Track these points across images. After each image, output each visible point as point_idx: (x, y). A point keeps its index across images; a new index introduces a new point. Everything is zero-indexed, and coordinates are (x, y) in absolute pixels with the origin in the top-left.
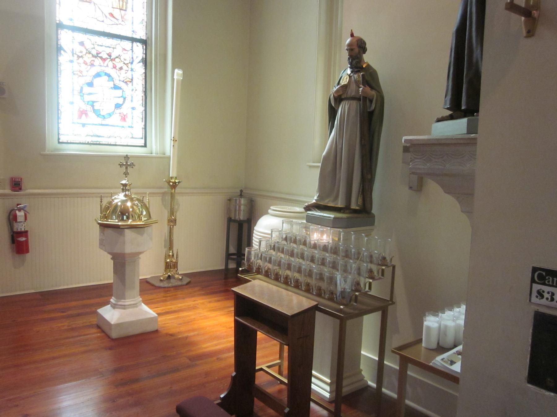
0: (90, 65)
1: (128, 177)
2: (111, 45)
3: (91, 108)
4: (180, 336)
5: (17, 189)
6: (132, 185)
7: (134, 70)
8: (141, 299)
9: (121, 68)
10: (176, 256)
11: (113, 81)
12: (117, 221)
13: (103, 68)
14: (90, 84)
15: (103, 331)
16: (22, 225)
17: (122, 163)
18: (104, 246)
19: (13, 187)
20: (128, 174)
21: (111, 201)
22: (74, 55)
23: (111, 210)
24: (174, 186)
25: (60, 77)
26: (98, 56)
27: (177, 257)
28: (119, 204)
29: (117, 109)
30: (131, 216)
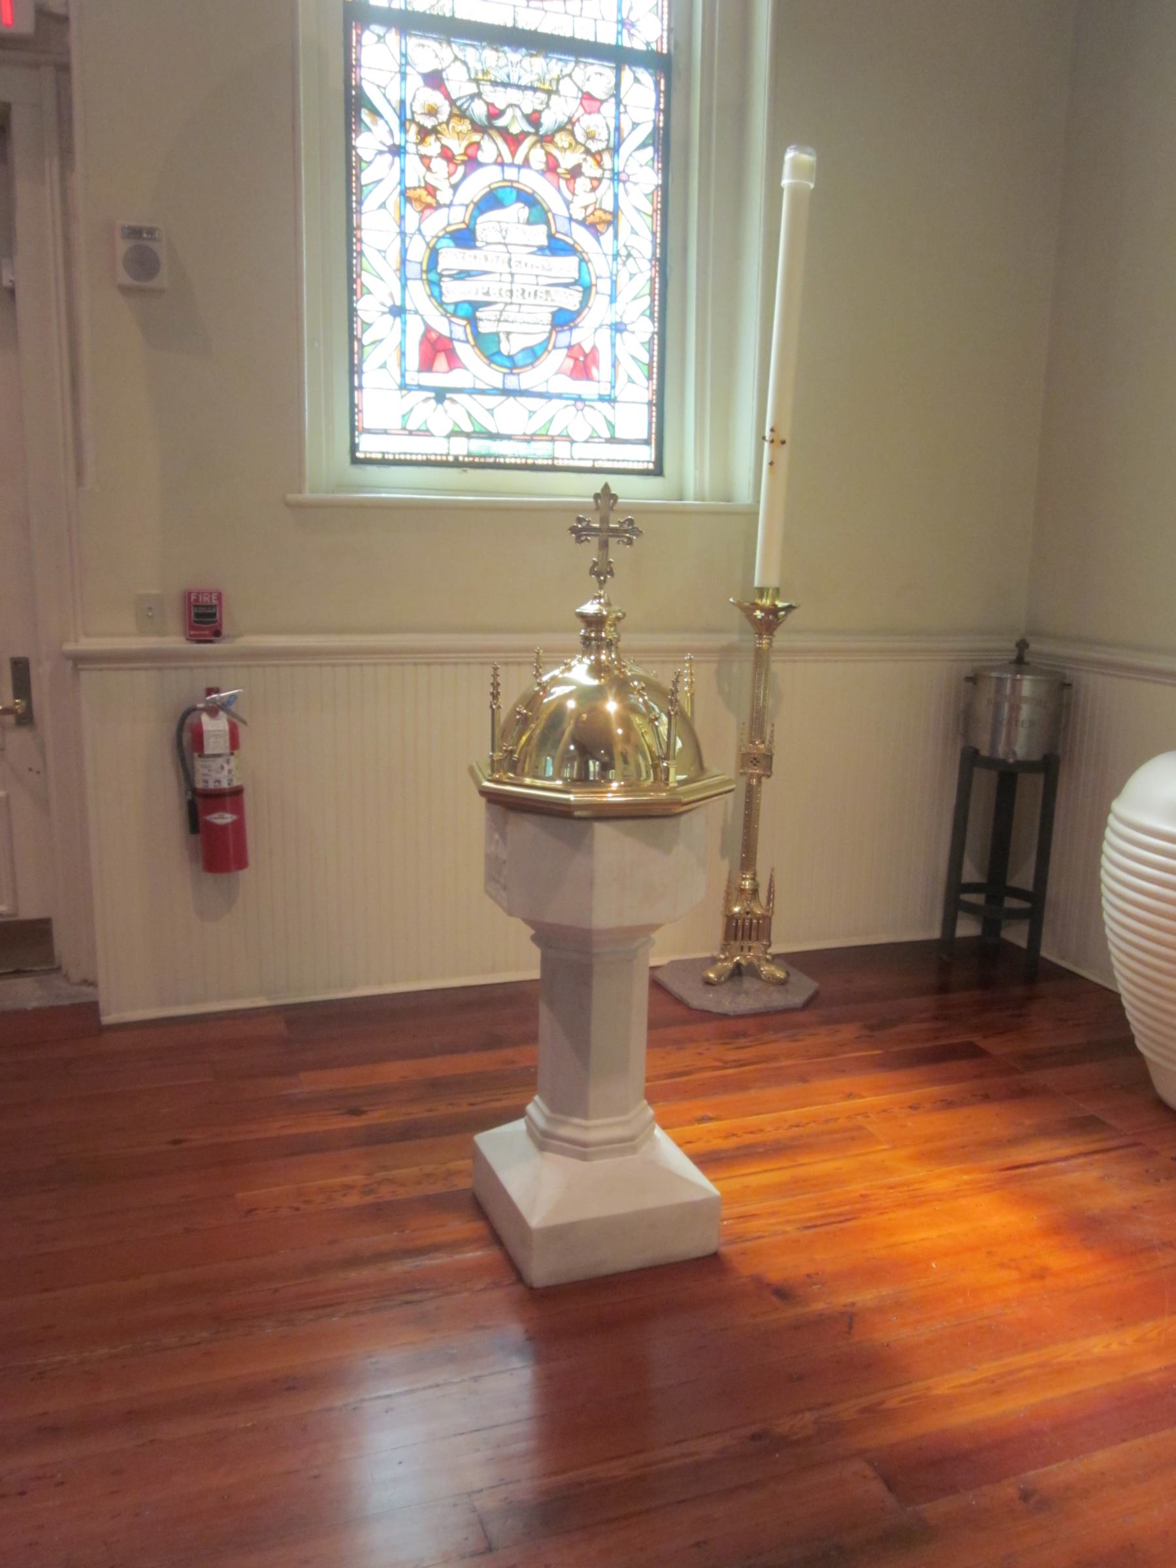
0: (463, 162)
1: (606, 586)
2: (539, 80)
3: (468, 329)
4: (819, 1306)
5: (207, 632)
6: (624, 622)
7: (623, 177)
8: (651, 1112)
9: (575, 172)
10: (766, 894)
11: (547, 223)
12: (559, 783)
13: (511, 173)
14: (465, 238)
15: (496, 1239)
16: (222, 768)
17: (584, 524)
18: (505, 888)
19: (191, 628)
20: (611, 573)
21: (538, 692)
22: (408, 124)
23: (538, 731)
24: (771, 622)
25: (360, 212)
26: (492, 127)
27: (770, 900)
28: (571, 704)
29: (559, 329)
30: (618, 762)
